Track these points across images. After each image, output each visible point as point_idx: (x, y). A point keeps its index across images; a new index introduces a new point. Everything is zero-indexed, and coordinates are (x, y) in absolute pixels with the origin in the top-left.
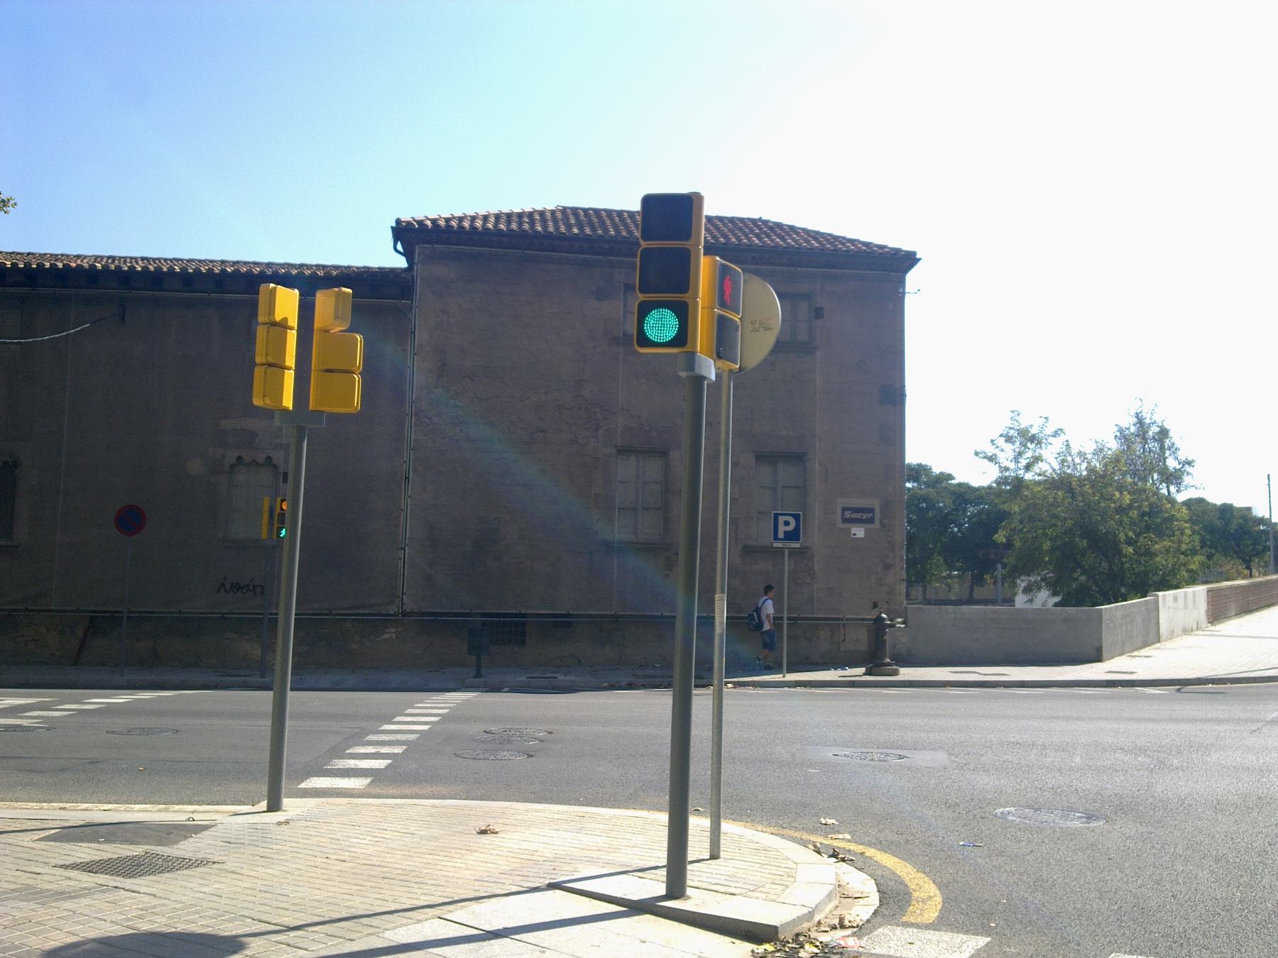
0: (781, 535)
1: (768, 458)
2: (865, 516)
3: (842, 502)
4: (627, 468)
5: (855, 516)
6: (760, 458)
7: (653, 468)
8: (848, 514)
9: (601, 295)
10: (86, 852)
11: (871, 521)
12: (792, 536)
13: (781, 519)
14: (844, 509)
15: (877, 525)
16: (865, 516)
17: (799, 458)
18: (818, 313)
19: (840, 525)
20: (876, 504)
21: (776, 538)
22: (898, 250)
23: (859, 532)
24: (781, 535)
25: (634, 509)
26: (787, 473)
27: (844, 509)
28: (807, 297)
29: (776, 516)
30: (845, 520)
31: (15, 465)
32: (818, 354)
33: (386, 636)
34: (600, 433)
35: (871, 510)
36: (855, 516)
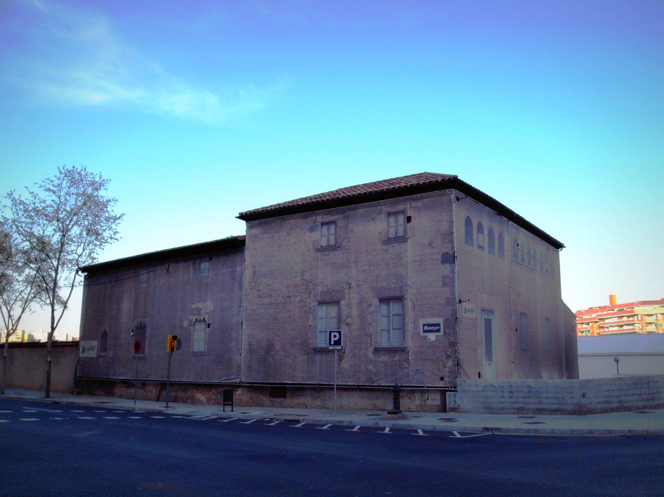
0: (332, 343)
1: (385, 300)
2: (435, 328)
3: (422, 321)
4: (322, 311)
5: (430, 328)
6: (382, 300)
7: (333, 310)
8: (426, 328)
9: (312, 230)
10: (373, 417)
11: (438, 331)
12: (338, 343)
13: (333, 334)
14: (424, 325)
15: (442, 333)
16: (435, 328)
17: (400, 299)
18: (409, 219)
19: (422, 334)
20: (440, 321)
21: (330, 344)
22: (505, 206)
23: (432, 337)
24: (332, 343)
25: (326, 332)
26: (395, 308)
27: (424, 325)
28: (403, 212)
29: (330, 333)
30: (425, 331)
31: (145, 327)
32: (409, 241)
33: (238, 392)
34: (311, 296)
35: (438, 325)
36: (430, 328)
